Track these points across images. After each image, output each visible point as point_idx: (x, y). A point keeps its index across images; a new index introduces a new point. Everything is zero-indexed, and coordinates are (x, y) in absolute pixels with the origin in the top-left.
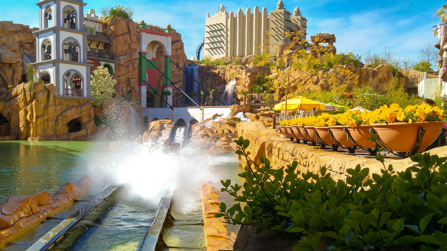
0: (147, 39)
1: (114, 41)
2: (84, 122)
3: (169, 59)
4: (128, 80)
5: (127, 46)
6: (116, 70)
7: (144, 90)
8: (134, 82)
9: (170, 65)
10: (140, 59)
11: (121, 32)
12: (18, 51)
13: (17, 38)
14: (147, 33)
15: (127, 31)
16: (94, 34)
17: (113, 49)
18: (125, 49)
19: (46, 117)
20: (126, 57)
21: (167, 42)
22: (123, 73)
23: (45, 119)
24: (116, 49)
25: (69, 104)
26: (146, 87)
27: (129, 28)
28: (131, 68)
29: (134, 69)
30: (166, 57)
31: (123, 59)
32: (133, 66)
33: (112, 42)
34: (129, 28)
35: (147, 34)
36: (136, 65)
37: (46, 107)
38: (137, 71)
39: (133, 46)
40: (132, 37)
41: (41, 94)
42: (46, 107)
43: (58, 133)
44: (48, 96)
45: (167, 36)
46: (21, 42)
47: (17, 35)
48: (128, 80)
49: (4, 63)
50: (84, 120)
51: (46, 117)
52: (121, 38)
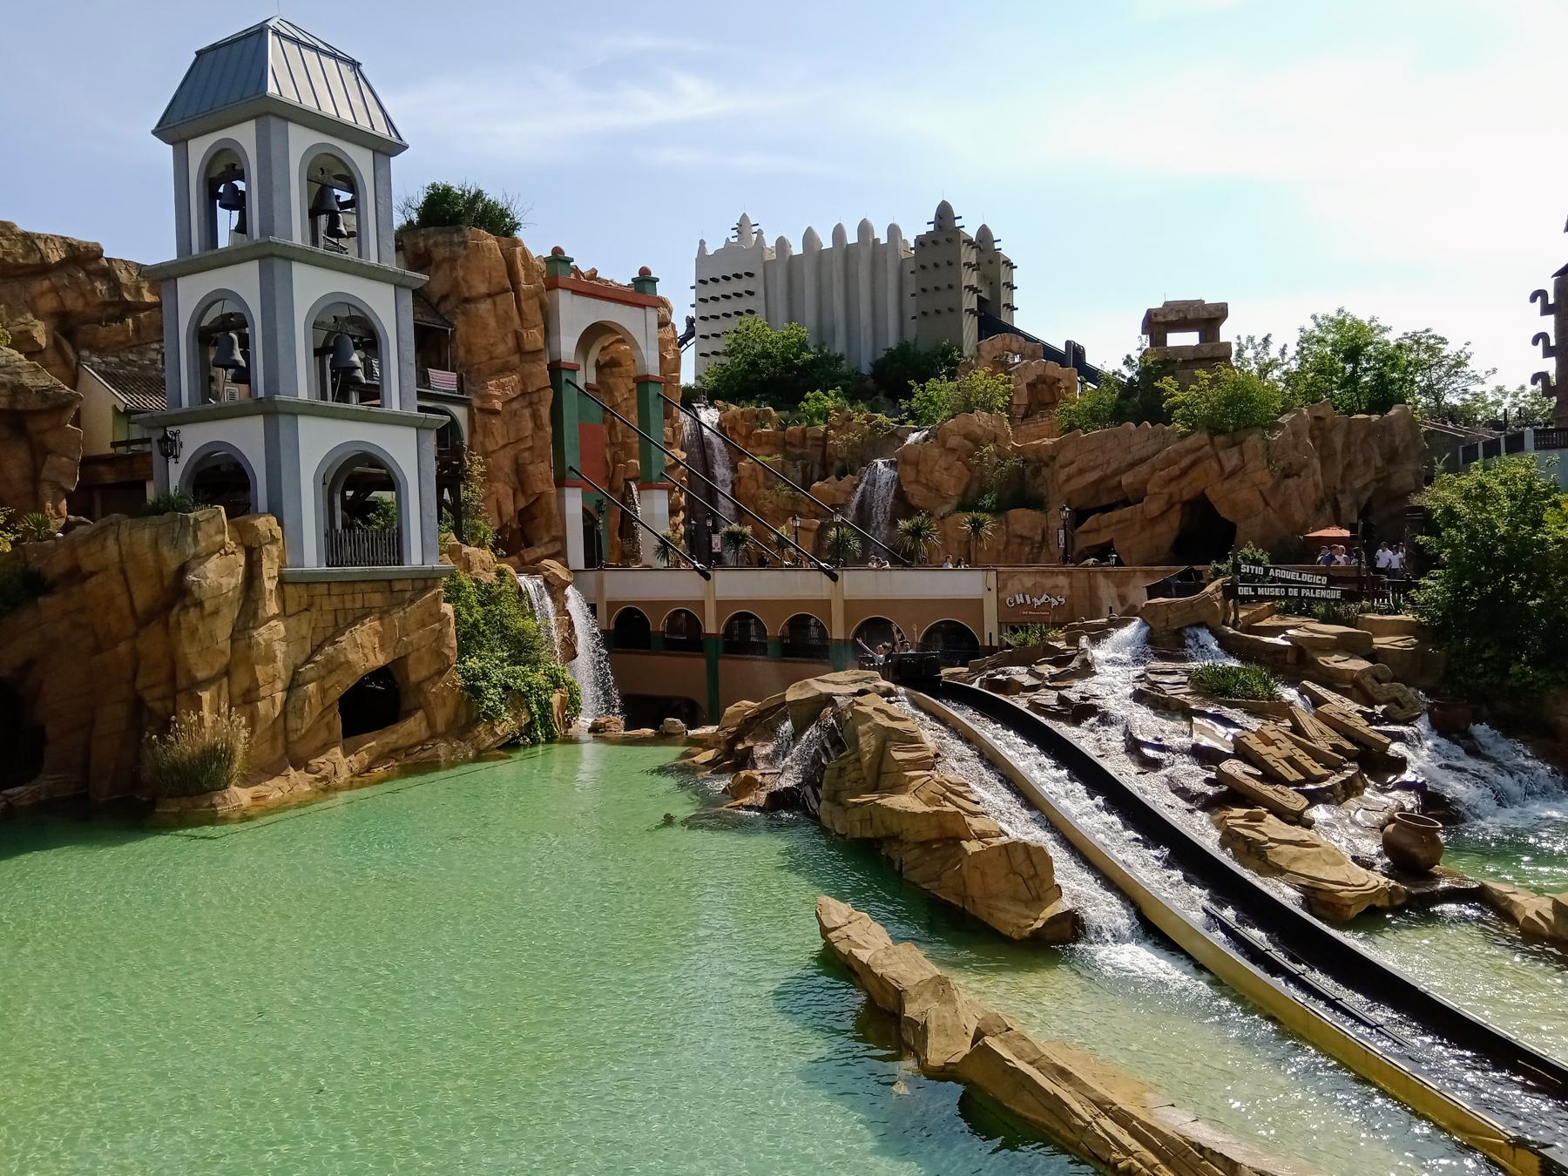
0: (574, 315)
1: (459, 322)
2: (413, 678)
3: (653, 390)
4: (519, 469)
5: (511, 342)
6: (473, 431)
7: (574, 503)
8: (542, 472)
11: (483, 288)
14: (575, 292)
15: (508, 284)
22: (501, 443)
23: (236, 690)
24: (469, 351)
25: (348, 605)
26: (579, 491)
28: (528, 425)
29: (538, 426)
30: (643, 381)
32: (535, 417)
33: (451, 325)
35: (576, 297)
36: (545, 412)
38: (549, 430)
39: (534, 338)
40: (524, 305)
45: (643, 306)
52: (484, 307)
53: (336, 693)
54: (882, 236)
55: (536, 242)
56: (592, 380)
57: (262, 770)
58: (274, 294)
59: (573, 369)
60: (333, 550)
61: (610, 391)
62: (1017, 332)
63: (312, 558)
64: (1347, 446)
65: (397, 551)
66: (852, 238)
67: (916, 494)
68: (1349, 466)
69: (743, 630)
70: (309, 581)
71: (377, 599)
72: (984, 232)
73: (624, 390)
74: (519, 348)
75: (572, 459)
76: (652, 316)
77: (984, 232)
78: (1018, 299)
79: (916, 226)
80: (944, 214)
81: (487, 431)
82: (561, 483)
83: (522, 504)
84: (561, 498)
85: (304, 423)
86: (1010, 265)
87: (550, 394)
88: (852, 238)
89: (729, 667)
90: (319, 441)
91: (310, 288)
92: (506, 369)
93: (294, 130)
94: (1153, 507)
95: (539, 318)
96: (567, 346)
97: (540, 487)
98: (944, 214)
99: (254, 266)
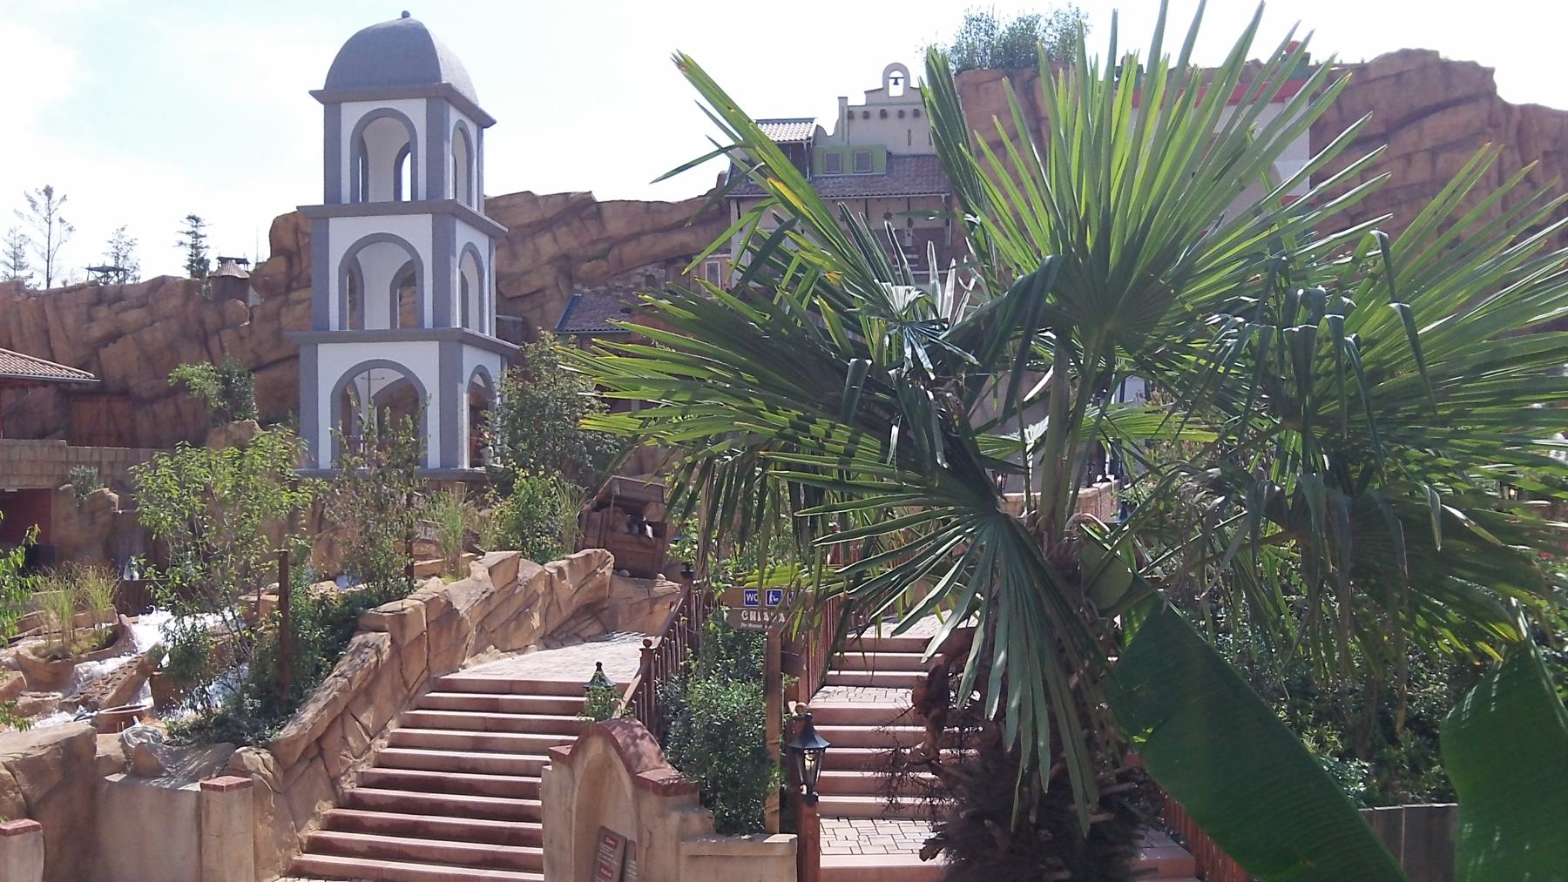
16: (880, 166)
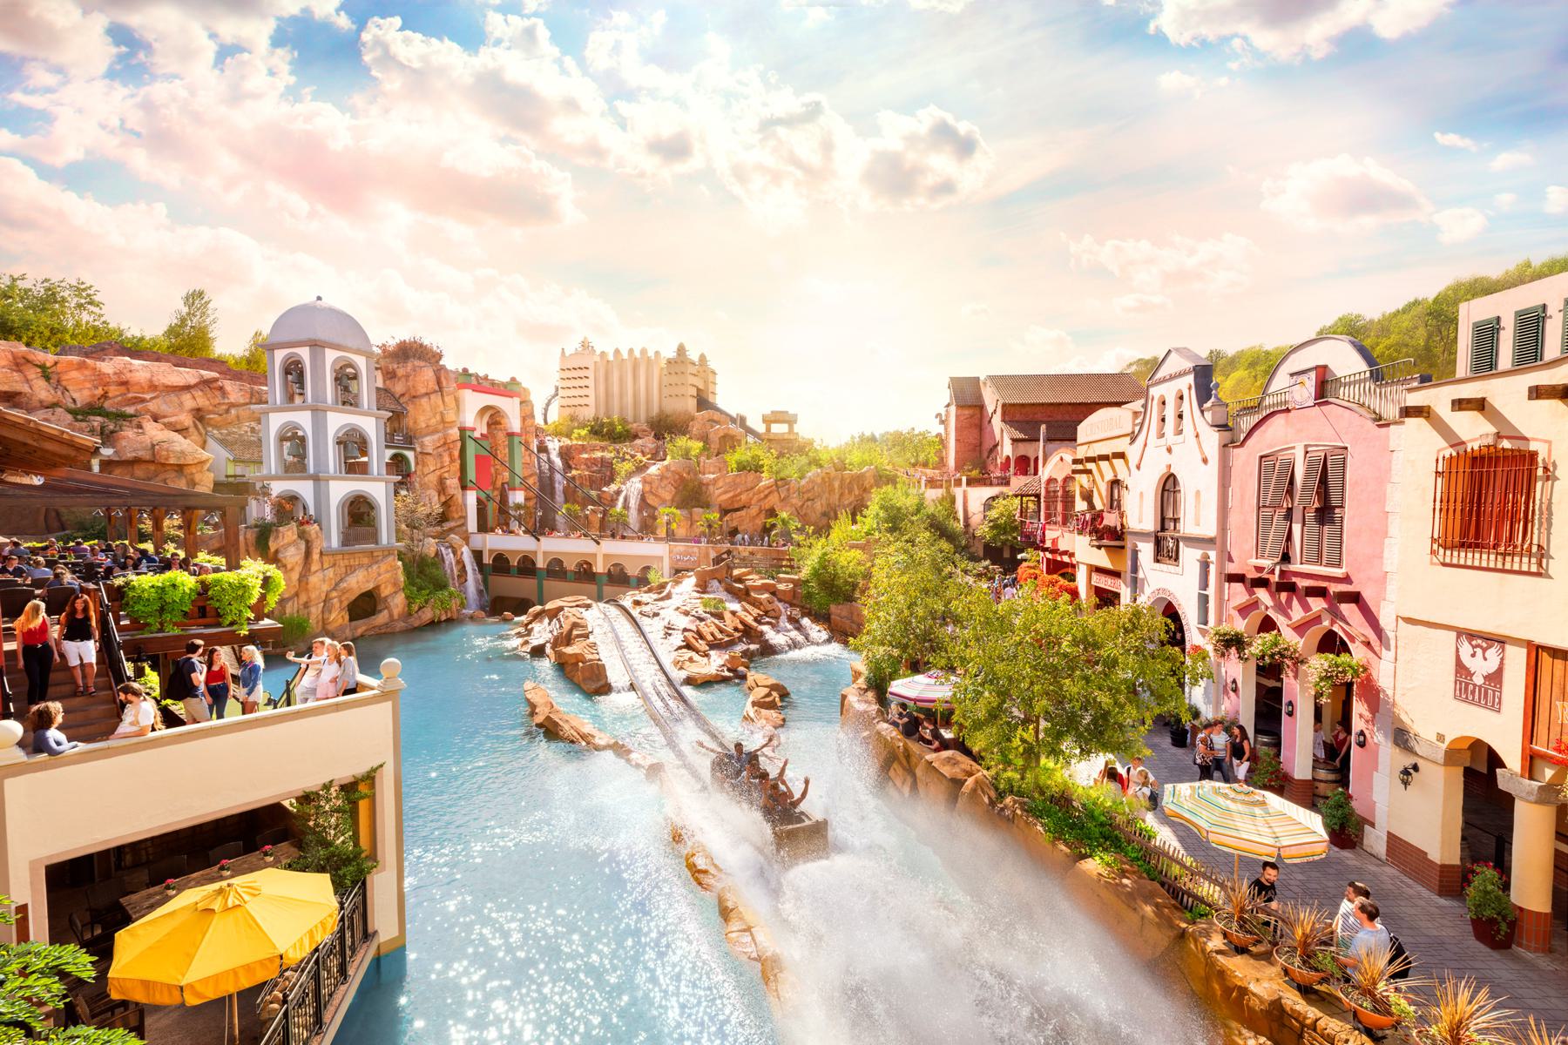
3: (516, 439)
4: (441, 481)
7: (471, 498)
8: (453, 483)
9: (519, 451)
10: (463, 439)
11: (423, 391)
12: (192, 429)
13: (188, 401)
17: (408, 422)
18: (433, 421)
19: (303, 598)
20: (436, 437)
21: (511, 409)
27: (439, 382)
28: (447, 459)
29: (452, 461)
30: (511, 435)
31: (429, 442)
32: (451, 455)
34: (439, 382)
36: (456, 453)
37: (303, 577)
39: (450, 416)
41: (292, 550)
42: (303, 577)
43: (330, 627)
44: (308, 554)
46: (198, 410)
47: (188, 396)
48: (441, 481)
49: (163, 465)
50: (386, 591)
51: (303, 598)
52: (424, 401)
53: (346, 603)
54: (651, 354)
55: (450, 362)
56: (485, 431)
57: (1324, 999)
58: (319, 425)
59: (473, 429)
60: (347, 540)
61: (494, 437)
62: (718, 410)
63: (335, 542)
64: (841, 487)
65: (374, 537)
66: (637, 354)
67: (651, 500)
68: (842, 495)
69: (557, 570)
70: (334, 554)
71: (366, 561)
72: (703, 358)
73: (501, 436)
74: (443, 421)
75: (471, 474)
76: (517, 400)
77: (703, 358)
78: (718, 389)
79: (669, 352)
80: (681, 350)
81: (424, 464)
82: (464, 488)
83: (443, 499)
84: (464, 496)
85: (332, 483)
86: (714, 373)
87: (459, 444)
88: (637, 354)
89: (551, 585)
90: (341, 489)
91: (337, 421)
92: (435, 431)
93: (327, 351)
94: (754, 511)
95: (453, 404)
96: (469, 418)
97: (452, 491)
98: (681, 350)
99: (309, 413)
